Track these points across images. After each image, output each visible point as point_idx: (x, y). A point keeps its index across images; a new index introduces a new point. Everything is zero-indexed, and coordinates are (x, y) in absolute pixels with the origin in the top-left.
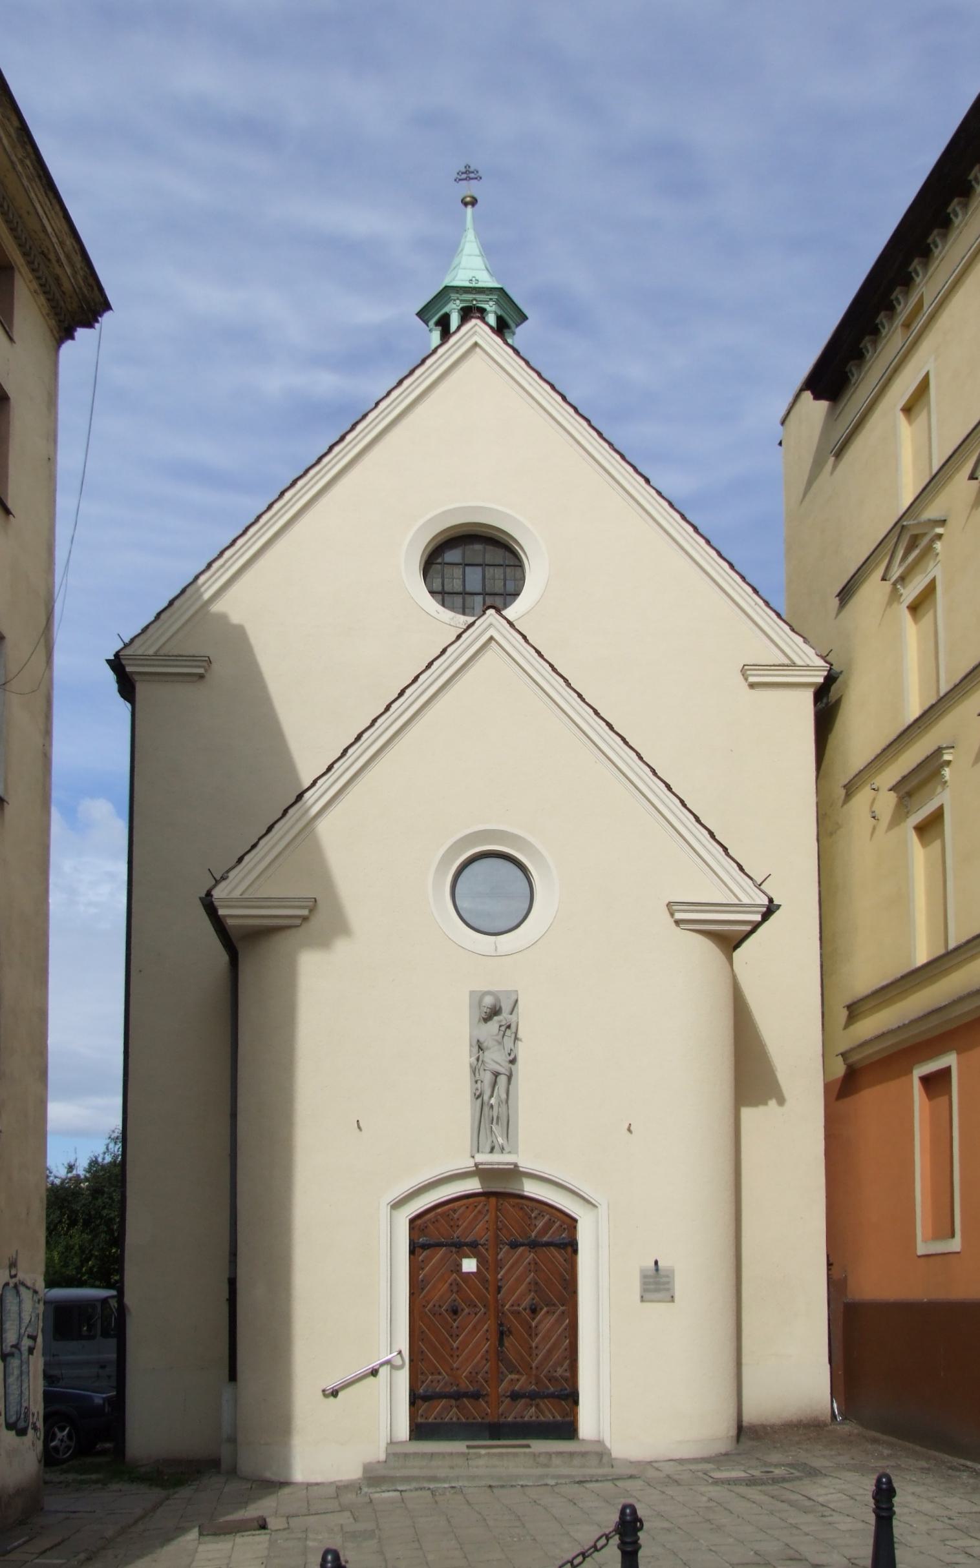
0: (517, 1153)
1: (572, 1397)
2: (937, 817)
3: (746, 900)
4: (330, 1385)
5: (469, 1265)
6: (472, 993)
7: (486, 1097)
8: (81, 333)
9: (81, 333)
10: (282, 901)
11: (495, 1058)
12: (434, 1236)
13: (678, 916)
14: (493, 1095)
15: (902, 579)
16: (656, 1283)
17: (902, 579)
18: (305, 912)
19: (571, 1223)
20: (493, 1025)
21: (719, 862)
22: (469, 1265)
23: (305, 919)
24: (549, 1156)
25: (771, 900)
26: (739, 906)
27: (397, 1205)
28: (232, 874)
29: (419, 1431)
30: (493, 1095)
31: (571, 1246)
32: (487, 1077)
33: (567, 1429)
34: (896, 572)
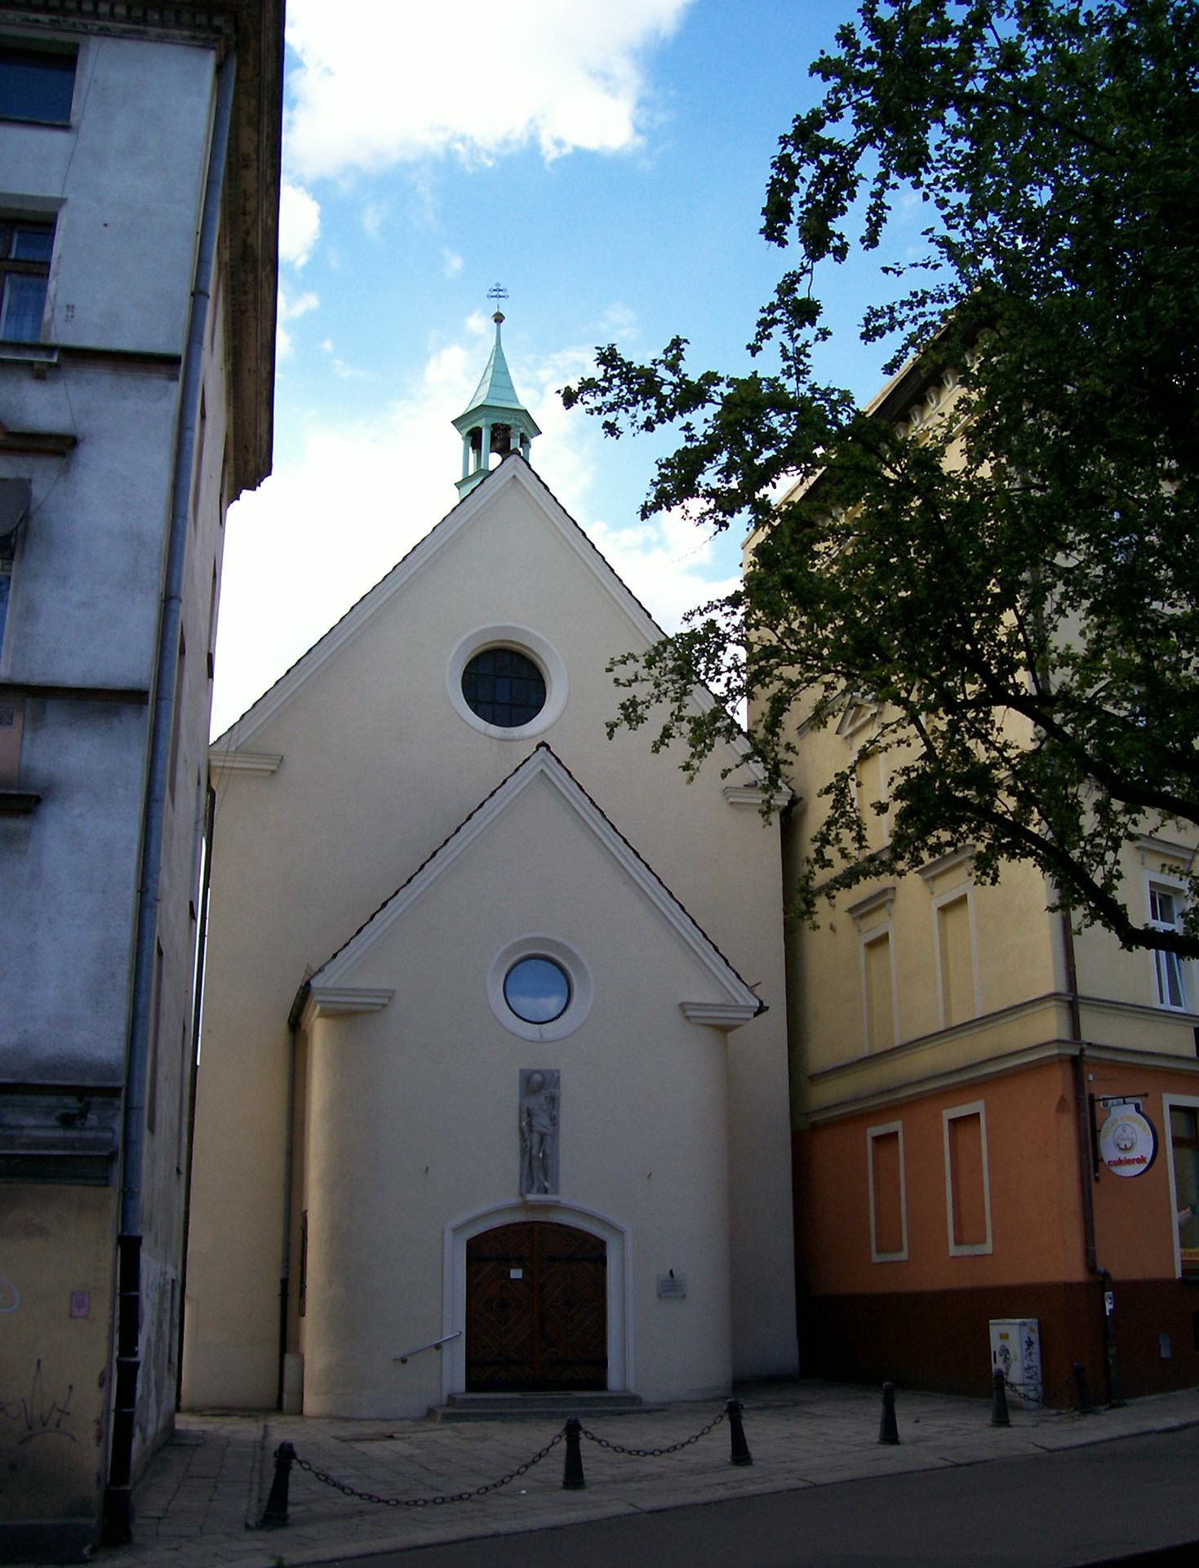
0: (557, 1192)
1: (603, 1363)
2: (884, 939)
3: (742, 1002)
4: (399, 1354)
5: (516, 1274)
6: (522, 1071)
7: (534, 1152)
8: (245, 494)
9: (245, 494)
10: (367, 992)
11: (541, 1121)
12: (487, 1253)
13: (689, 1013)
14: (538, 1157)
15: (852, 735)
16: (671, 1286)
17: (852, 735)
18: (385, 1001)
19: (602, 1244)
20: (542, 1098)
21: (719, 969)
22: (516, 1274)
23: (385, 1006)
24: (581, 1194)
25: (761, 1003)
26: (737, 1007)
27: (455, 1230)
28: (327, 968)
29: (471, 1386)
30: (538, 1157)
31: (603, 1261)
32: (536, 1138)
33: (601, 1383)
34: (848, 731)
